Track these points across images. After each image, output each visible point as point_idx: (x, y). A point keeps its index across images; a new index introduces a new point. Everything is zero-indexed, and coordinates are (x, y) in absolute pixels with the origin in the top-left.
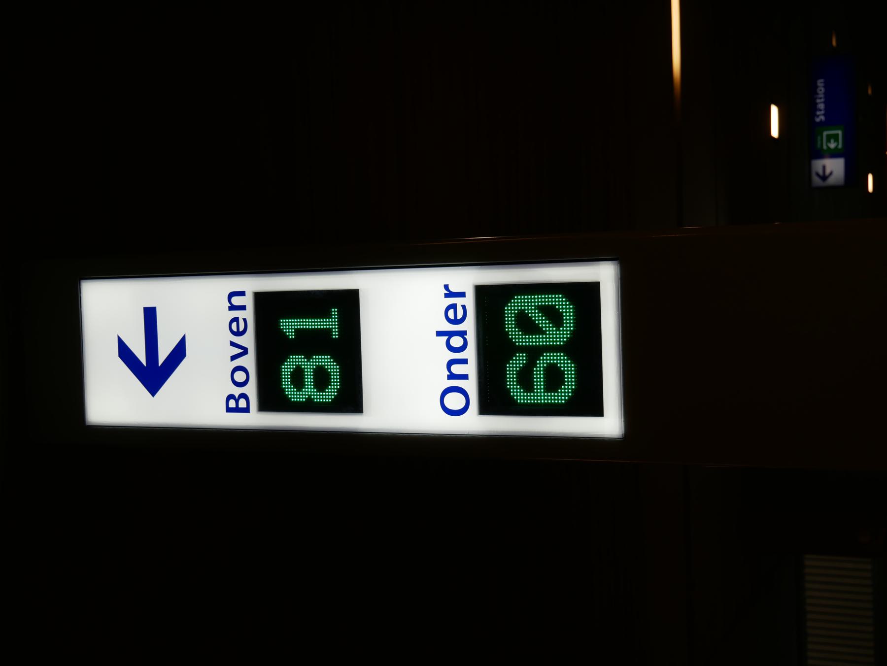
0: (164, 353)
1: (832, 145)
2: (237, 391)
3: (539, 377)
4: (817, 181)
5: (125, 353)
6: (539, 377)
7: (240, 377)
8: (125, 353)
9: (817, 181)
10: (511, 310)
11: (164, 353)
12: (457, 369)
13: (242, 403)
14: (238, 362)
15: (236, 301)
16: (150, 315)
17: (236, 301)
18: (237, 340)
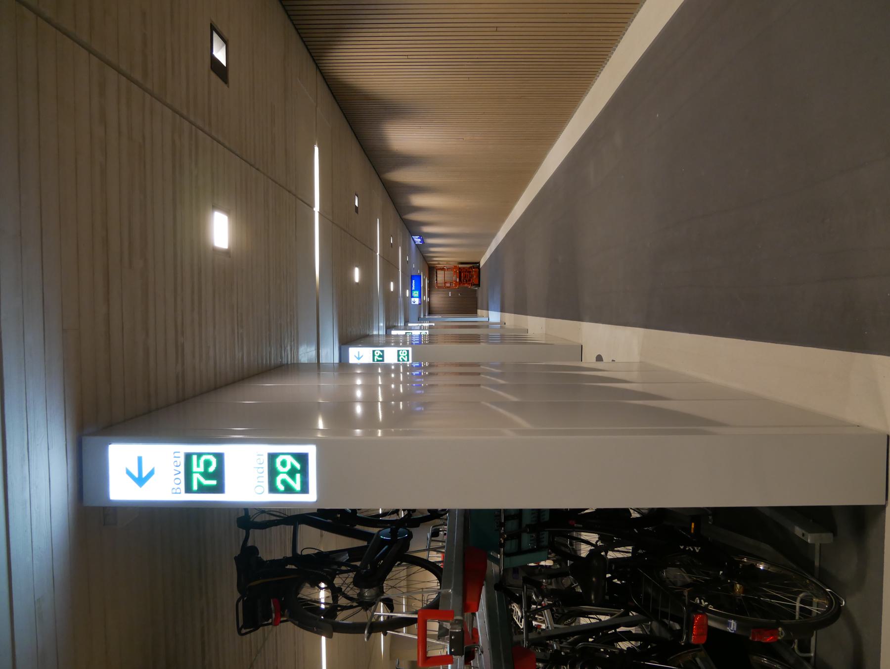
0: (144, 474)
1: (416, 295)
2: (176, 486)
3: (403, 353)
4: (412, 303)
5: (129, 473)
6: (403, 353)
7: (177, 481)
8: (129, 473)
9: (412, 303)
10: (278, 461)
11: (144, 474)
12: (260, 479)
13: (178, 491)
14: (177, 476)
15: (176, 455)
16: (140, 460)
17: (176, 455)
18: (176, 468)
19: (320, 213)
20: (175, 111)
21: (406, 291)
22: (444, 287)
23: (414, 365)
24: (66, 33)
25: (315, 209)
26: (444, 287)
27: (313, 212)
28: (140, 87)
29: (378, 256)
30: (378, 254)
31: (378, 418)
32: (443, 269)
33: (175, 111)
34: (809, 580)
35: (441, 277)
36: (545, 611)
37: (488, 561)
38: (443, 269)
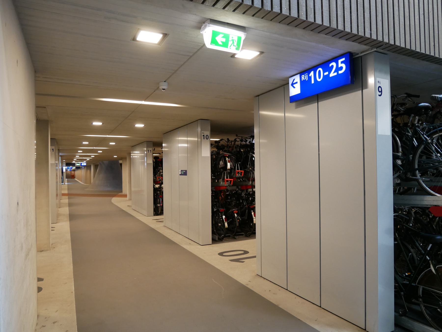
19: (107, 137)
20: (182, 66)
21: (88, 142)
22: (71, 173)
23: (162, 173)
24: (184, 63)
25: (143, 101)
26: (71, 173)
27: (106, 135)
28: (168, 78)
29: (93, 148)
30: (94, 148)
31: (167, 150)
32: (74, 173)
33: (182, 66)
34: (416, 229)
35: (73, 172)
36: (131, 155)
37: (330, 76)
38: (74, 173)
